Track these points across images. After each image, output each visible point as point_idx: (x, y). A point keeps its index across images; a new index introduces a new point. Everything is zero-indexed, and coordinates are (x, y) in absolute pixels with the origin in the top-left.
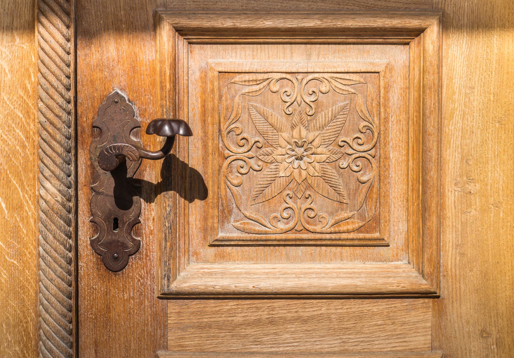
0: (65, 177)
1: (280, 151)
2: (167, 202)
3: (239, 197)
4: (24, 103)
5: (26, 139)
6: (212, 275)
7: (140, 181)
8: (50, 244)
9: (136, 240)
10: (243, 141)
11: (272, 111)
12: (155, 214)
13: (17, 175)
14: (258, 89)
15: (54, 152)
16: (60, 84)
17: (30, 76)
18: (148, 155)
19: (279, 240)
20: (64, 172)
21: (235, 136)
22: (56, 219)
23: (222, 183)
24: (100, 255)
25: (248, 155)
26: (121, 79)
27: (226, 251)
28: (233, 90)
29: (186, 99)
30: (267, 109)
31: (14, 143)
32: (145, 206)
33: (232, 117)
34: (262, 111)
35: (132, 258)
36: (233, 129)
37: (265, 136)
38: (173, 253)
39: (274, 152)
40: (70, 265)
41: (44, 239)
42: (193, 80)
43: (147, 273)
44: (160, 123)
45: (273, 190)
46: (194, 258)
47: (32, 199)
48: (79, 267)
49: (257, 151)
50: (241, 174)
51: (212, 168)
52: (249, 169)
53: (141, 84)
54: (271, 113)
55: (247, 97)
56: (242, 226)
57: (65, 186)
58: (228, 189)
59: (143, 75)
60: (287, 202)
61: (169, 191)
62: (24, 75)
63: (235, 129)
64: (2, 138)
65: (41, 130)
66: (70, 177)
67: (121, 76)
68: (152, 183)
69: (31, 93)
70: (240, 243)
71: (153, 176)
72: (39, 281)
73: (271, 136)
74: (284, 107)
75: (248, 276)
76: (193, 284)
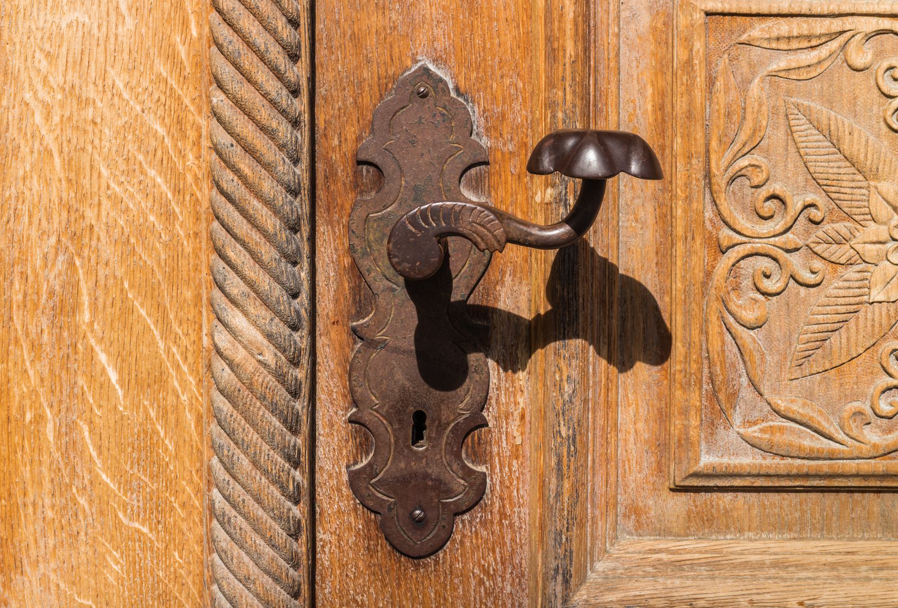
0: (285, 298)
1: (873, 230)
2: (564, 369)
3: (757, 356)
4: (171, 95)
5: (174, 195)
6: (683, 570)
7: (486, 313)
8: (244, 480)
9: (474, 472)
10: (772, 205)
11: (852, 120)
12: (528, 401)
13: (151, 293)
14: (815, 61)
15: (254, 230)
16: (272, 40)
17: (185, 24)
18: (530, 234)
19: (866, 477)
20: (281, 284)
21: (749, 191)
22: (261, 413)
23: (714, 318)
24: (376, 513)
25: (785, 243)
26: (435, 31)
27: (718, 505)
28: (744, 64)
29: (613, 87)
30: (839, 117)
31: (143, 205)
32: (499, 379)
33: (743, 137)
34: (824, 121)
35: (463, 522)
36: (743, 172)
37: (833, 189)
38: (578, 509)
39: (857, 234)
40: (297, 540)
41: (226, 469)
42: (632, 35)
43: (503, 564)
44: (570, 143)
45: (853, 339)
46: (631, 524)
47: (190, 359)
48: (319, 544)
49: (808, 232)
50: (763, 294)
51: (684, 277)
52: (786, 280)
53: (492, 44)
54: (850, 126)
55: (783, 83)
56: (767, 436)
57: (286, 322)
58: (728, 334)
59: (498, 20)
60: (891, 371)
61: (570, 338)
62: (169, 21)
63: (749, 172)
64: (109, 192)
65: (218, 167)
66: (298, 300)
67: (435, 23)
68: (519, 318)
69: (188, 70)
70: (759, 483)
71: (522, 297)
72: (212, 583)
73: (848, 191)
74: (885, 111)
75: (782, 574)
76: (633, 593)
